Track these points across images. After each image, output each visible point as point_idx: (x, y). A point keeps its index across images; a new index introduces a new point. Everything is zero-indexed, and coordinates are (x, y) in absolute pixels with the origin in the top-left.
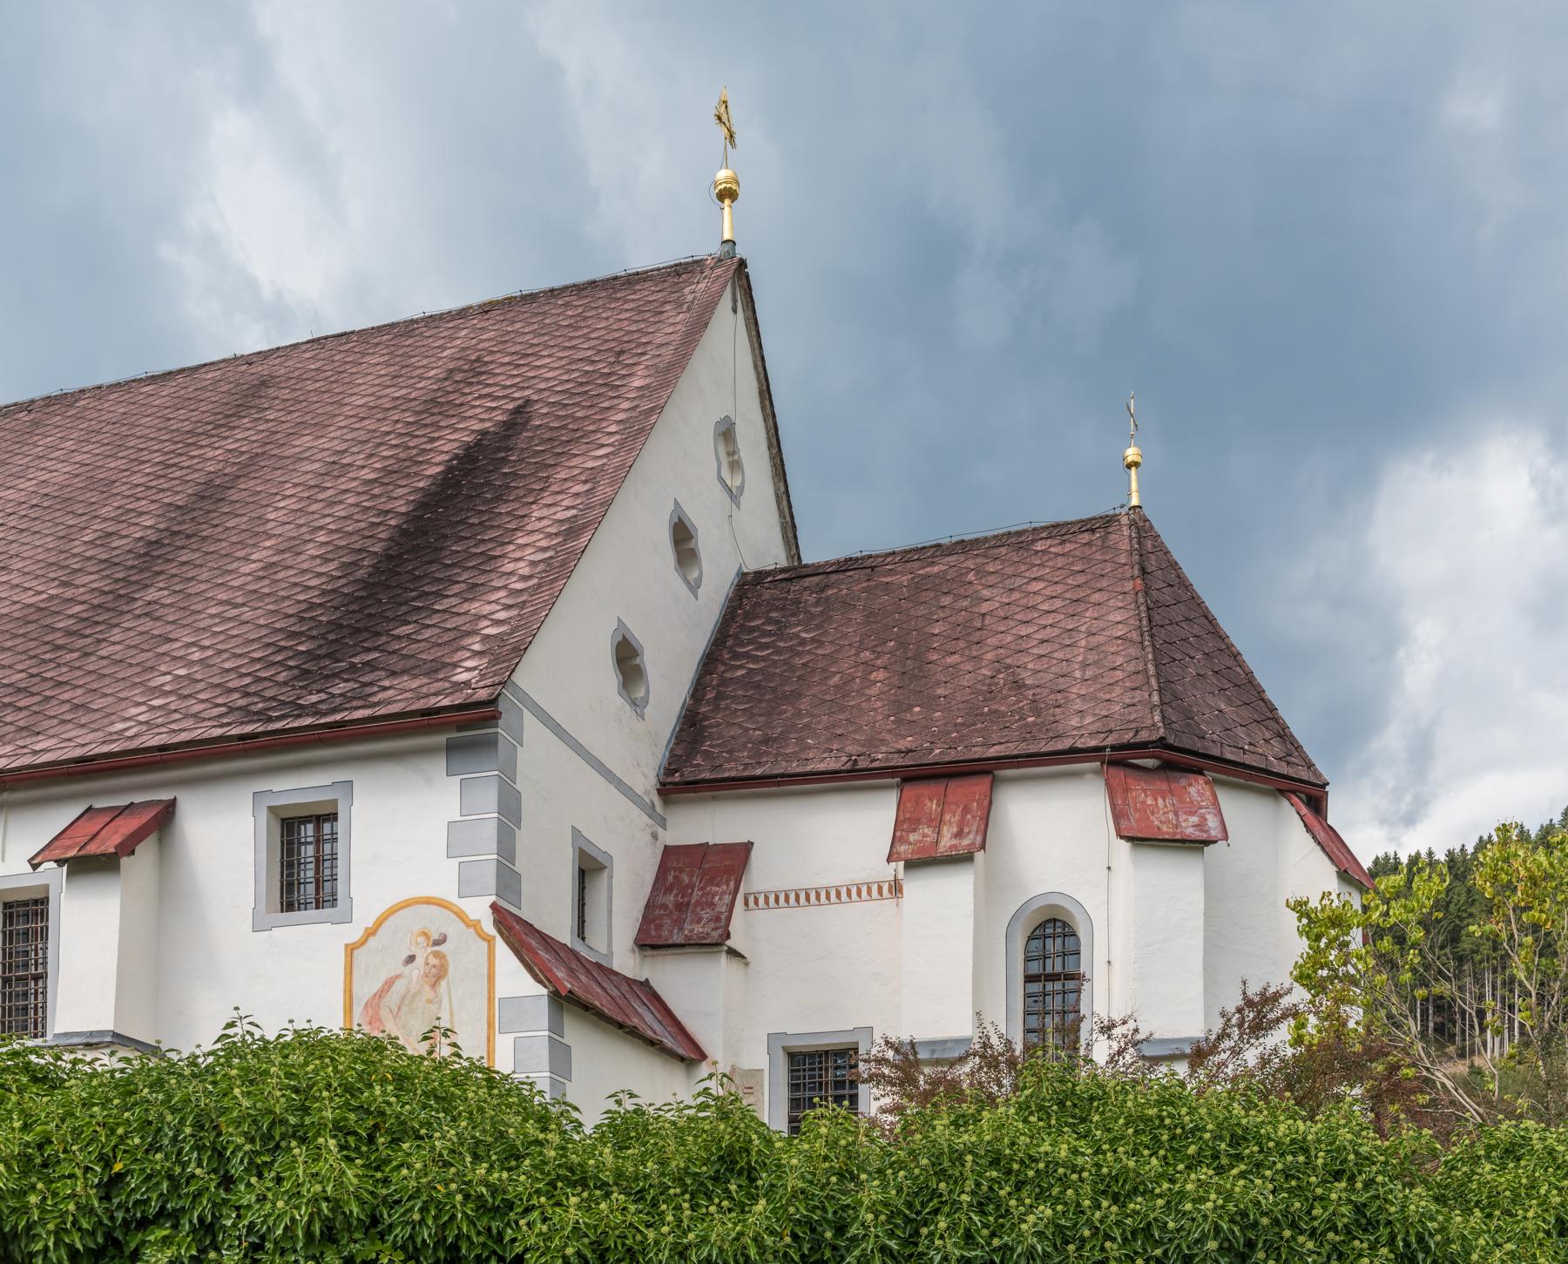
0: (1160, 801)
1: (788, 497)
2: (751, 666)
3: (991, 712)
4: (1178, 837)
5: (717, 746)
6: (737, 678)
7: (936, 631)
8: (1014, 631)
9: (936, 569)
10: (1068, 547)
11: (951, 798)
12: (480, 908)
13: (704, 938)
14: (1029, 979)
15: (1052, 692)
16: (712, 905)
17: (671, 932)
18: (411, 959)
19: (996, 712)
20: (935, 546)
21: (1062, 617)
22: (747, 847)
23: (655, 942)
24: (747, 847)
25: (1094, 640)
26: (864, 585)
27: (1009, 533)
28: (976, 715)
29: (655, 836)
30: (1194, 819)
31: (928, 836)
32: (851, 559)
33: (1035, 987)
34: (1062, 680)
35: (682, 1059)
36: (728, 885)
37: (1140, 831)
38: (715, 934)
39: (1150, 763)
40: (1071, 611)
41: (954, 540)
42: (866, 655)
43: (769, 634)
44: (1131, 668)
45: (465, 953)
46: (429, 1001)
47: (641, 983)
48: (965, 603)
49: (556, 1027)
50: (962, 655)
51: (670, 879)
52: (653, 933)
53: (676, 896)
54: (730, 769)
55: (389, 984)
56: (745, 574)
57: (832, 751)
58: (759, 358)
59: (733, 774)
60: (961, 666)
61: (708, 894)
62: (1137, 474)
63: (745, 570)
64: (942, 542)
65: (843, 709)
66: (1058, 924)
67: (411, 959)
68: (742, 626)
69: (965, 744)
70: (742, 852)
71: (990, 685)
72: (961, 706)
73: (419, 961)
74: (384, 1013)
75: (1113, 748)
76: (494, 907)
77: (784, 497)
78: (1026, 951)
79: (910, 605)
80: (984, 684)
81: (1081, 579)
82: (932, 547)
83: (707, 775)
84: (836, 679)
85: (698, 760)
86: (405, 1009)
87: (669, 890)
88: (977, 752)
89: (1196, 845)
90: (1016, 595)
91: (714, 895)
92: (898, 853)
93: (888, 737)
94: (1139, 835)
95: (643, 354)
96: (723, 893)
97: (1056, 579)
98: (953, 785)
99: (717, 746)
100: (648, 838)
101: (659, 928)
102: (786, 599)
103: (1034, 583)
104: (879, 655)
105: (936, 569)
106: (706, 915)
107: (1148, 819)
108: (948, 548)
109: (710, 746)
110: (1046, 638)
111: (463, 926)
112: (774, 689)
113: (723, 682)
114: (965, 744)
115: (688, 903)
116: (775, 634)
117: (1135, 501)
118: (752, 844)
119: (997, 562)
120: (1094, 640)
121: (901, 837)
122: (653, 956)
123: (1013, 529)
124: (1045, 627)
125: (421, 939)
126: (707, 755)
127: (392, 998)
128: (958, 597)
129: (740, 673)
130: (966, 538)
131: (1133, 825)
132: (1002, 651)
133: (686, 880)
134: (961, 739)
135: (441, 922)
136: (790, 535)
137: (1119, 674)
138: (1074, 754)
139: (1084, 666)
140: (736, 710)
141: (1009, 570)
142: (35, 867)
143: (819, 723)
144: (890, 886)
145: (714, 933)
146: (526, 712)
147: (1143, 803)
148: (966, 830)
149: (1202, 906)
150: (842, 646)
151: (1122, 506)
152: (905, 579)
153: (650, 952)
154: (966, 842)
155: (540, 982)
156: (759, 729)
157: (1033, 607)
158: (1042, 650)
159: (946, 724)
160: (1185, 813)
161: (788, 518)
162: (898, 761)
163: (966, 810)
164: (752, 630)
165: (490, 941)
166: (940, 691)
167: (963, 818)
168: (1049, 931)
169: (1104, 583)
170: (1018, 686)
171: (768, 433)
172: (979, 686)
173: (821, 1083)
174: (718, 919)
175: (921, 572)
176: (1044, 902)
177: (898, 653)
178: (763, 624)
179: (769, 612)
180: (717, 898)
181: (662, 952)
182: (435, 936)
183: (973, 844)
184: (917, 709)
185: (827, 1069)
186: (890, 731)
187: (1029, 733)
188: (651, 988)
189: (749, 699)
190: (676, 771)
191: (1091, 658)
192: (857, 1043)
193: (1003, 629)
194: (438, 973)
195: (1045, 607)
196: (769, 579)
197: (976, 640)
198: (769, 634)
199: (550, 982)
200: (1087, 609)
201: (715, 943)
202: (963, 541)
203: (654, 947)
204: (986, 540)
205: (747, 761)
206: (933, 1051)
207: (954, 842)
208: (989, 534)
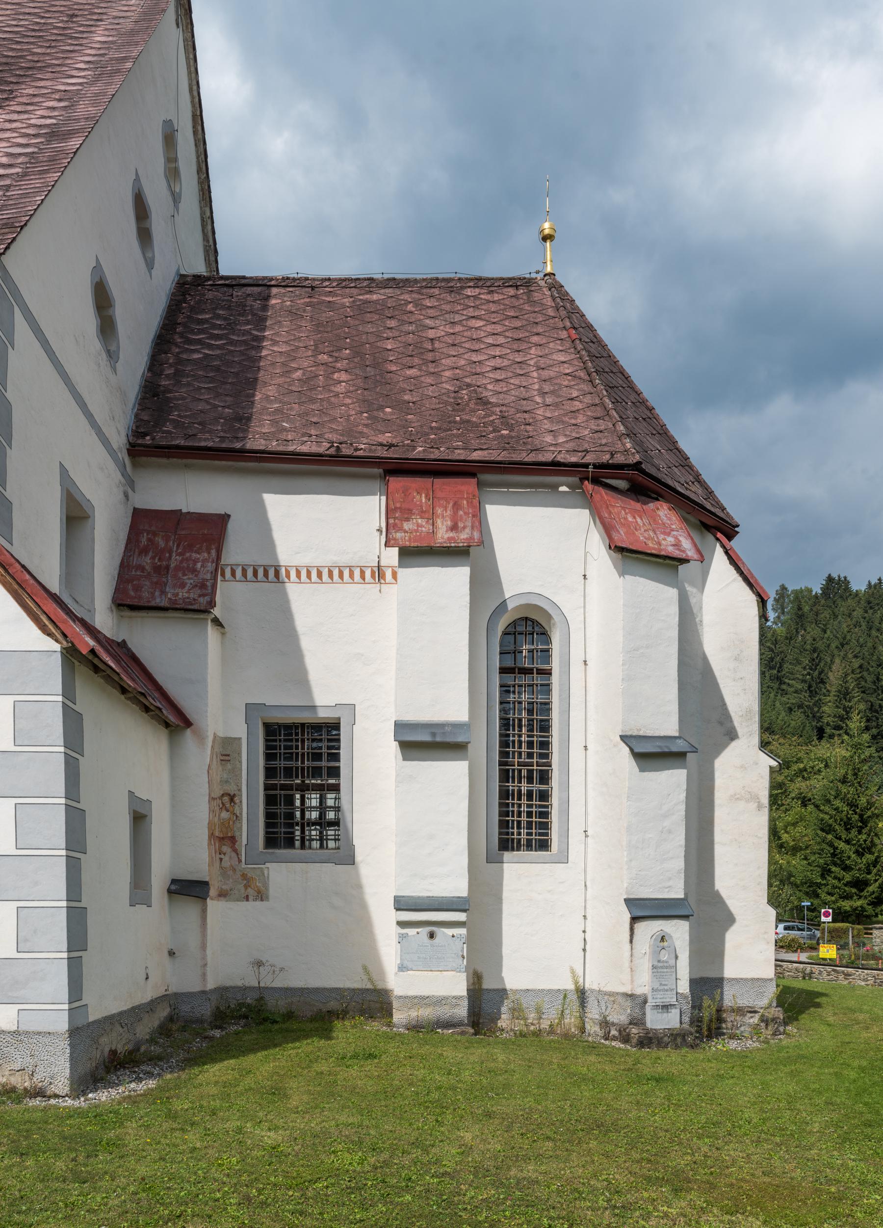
0: (639, 520)
1: (213, 222)
2: (207, 352)
3: (463, 422)
4: (663, 553)
5: (186, 417)
6: (194, 360)
7: (389, 347)
8: (466, 356)
9: (375, 297)
10: (496, 297)
11: (439, 494)
13: (192, 604)
14: (503, 670)
15: (518, 411)
16: (194, 571)
17: (153, 594)
19: (468, 421)
20: (369, 279)
21: (509, 351)
22: (224, 519)
23: (135, 602)
24: (224, 519)
25: (546, 374)
26: (308, 300)
27: (437, 279)
28: (450, 422)
29: (126, 496)
30: (670, 539)
31: (422, 526)
32: (288, 278)
33: (509, 679)
34: (525, 402)
35: (167, 725)
36: (209, 553)
37: (632, 544)
38: (203, 601)
39: (622, 484)
40: (515, 347)
41: (386, 276)
42: (324, 358)
43: (220, 327)
44: (588, 399)
47: (118, 644)
48: (412, 328)
49: (68, 692)
50: (420, 370)
51: (144, 540)
52: (132, 593)
53: (153, 558)
54: (205, 440)
56: (182, 276)
57: (311, 436)
58: (194, 82)
59: (210, 444)
60: (422, 379)
61: (187, 560)
62: (550, 245)
63: (183, 272)
64: (375, 276)
65: (312, 400)
66: (529, 623)
68: (189, 317)
69: (447, 445)
71: (455, 398)
72: (432, 412)
75: (595, 466)
77: (209, 222)
78: (501, 645)
79: (357, 322)
80: (449, 397)
81: (518, 323)
82: (365, 279)
83: (182, 442)
84: (298, 374)
85: (169, 427)
87: (144, 551)
88: (459, 454)
90: (458, 328)
91: (195, 561)
92: (395, 539)
93: (365, 430)
94: (631, 547)
95: (101, 20)
96: (205, 561)
97: (495, 320)
98: (438, 481)
99: (186, 417)
100: (121, 496)
101: (137, 589)
102: (231, 301)
103: (474, 321)
104: (337, 360)
105: (375, 297)
106: (189, 580)
107: (634, 534)
108: (381, 282)
109: (179, 416)
110: (498, 366)
112: (236, 374)
113: (179, 361)
114: (447, 445)
115: (167, 568)
116: (225, 329)
117: (549, 269)
118: (229, 516)
119: (432, 299)
120: (546, 374)
121: (395, 525)
122: (130, 617)
123: (440, 276)
124: (495, 357)
126: (177, 424)
128: (403, 322)
129: (196, 356)
130: (397, 276)
131: (622, 538)
132: (458, 371)
133: (162, 544)
134: (442, 441)
136: (212, 258)
137: (577, 405)
138: (556, 467)
139: (543, 394)
140: (200, 388)
141: (447, 307)
143: (291, 409)
144: (373, 573)
145: (201, 600)
146: (17, 309)
147: (626, 519)
148: (461, 525)
149: (677, 619)
150: (298, 348)
151: (538, 272)
152: (347, 301)
153: (128, 613)
154: (464, 535)
155: (50, 634)
156: (228, 407)
157: (478, 340)
158: (498, 375)
159: (421, 426)
160: (662, 533)
161: (211, 242)
162: (381, 452)
163: (457, 506)
164: (201, 322)
166: (406, 397)
167: (455, 513)
168: (519, 629)
169: (540, 329)
170: (483, 402)
171: (198, 158)
172: (445, 398)
173: (297, 754)
174: (203, 586)
175: (361, 297)
176: (523, 601)
177: (356, 360)
178: (211, 318)
179: (216, 309)
180: (199, 565)
181: (190, 615)
183: (471, 538)
184: (388, 410)
185: (303, 741)
186: (366, 425)
187: (506, 444)
188: (129, 650)
189: (212, 380)
190: (147, 435)
191: (547, 388)
192: (339, 719)
193: (454, 354)
195: (490, 340)
196: (209, 283)
197: (430, 359)
198: (220, 327)
199: (65, 636)
200: (530, 348)
202: (394, 279)
203: (133, 608)
204: (416, 281)
205: (222, 434)
206: (434, 735)
207: (451, 534)
208: (418, 277)
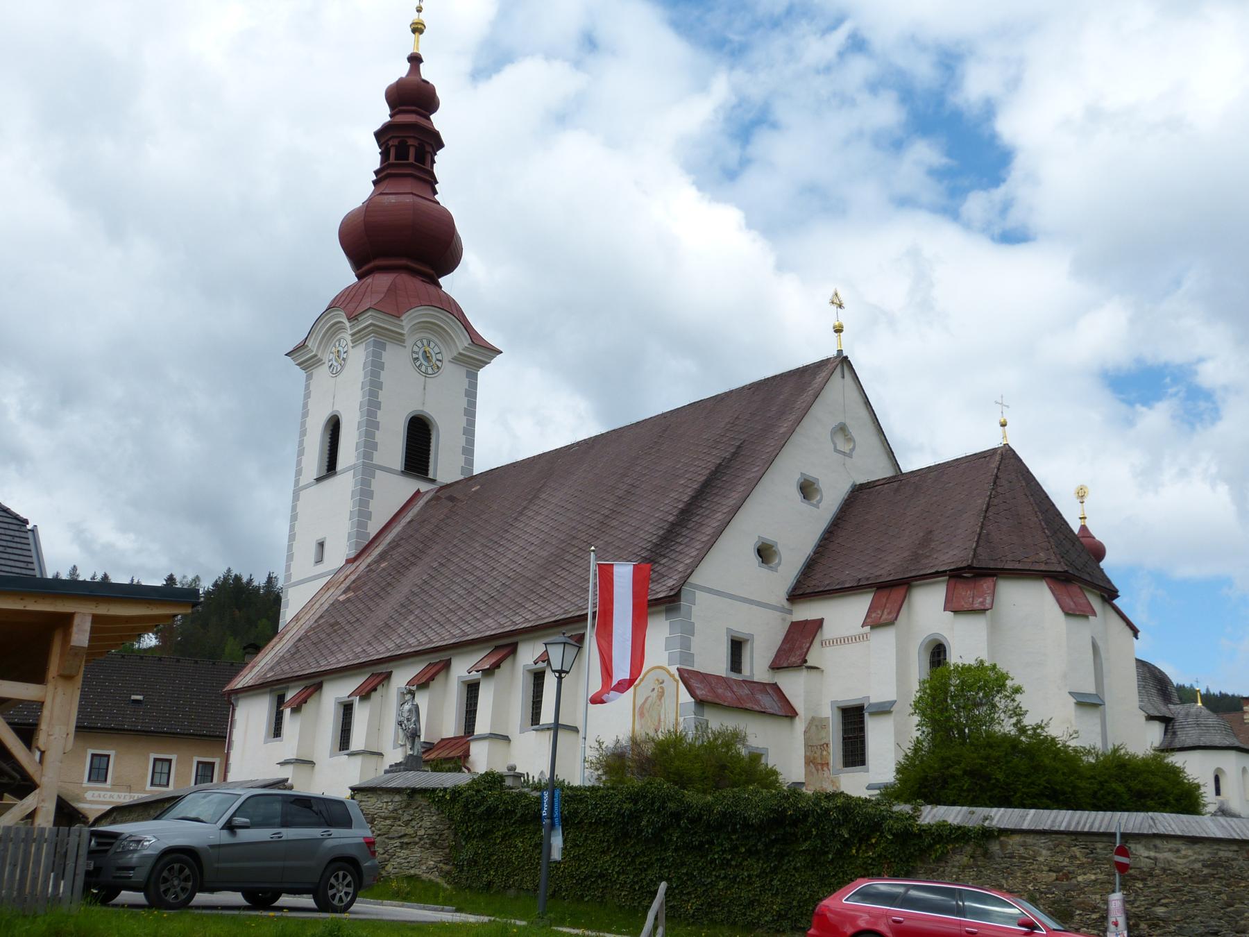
12: (673, 670)
18: (654, 689)
45: (670, 686)
46: (659, 706)
55: (647, 699)
56: (856, 485)
67: (654, 689)
70: (819, 624)
73: (656, 690)
74: (645, 711)
76: (678, 669)
86: (651, 709)
89: (983, 611)
111: (669, 676)
125: (657, 682)
127: (647, 706)
135: (663, 675)
136: (892, 456)
138: (938, 574)
142: (536, 664)
165: (677, 681)
182: (661, 681)
194: (661, 695)
201: (802, 664)
203: (778, 669)
